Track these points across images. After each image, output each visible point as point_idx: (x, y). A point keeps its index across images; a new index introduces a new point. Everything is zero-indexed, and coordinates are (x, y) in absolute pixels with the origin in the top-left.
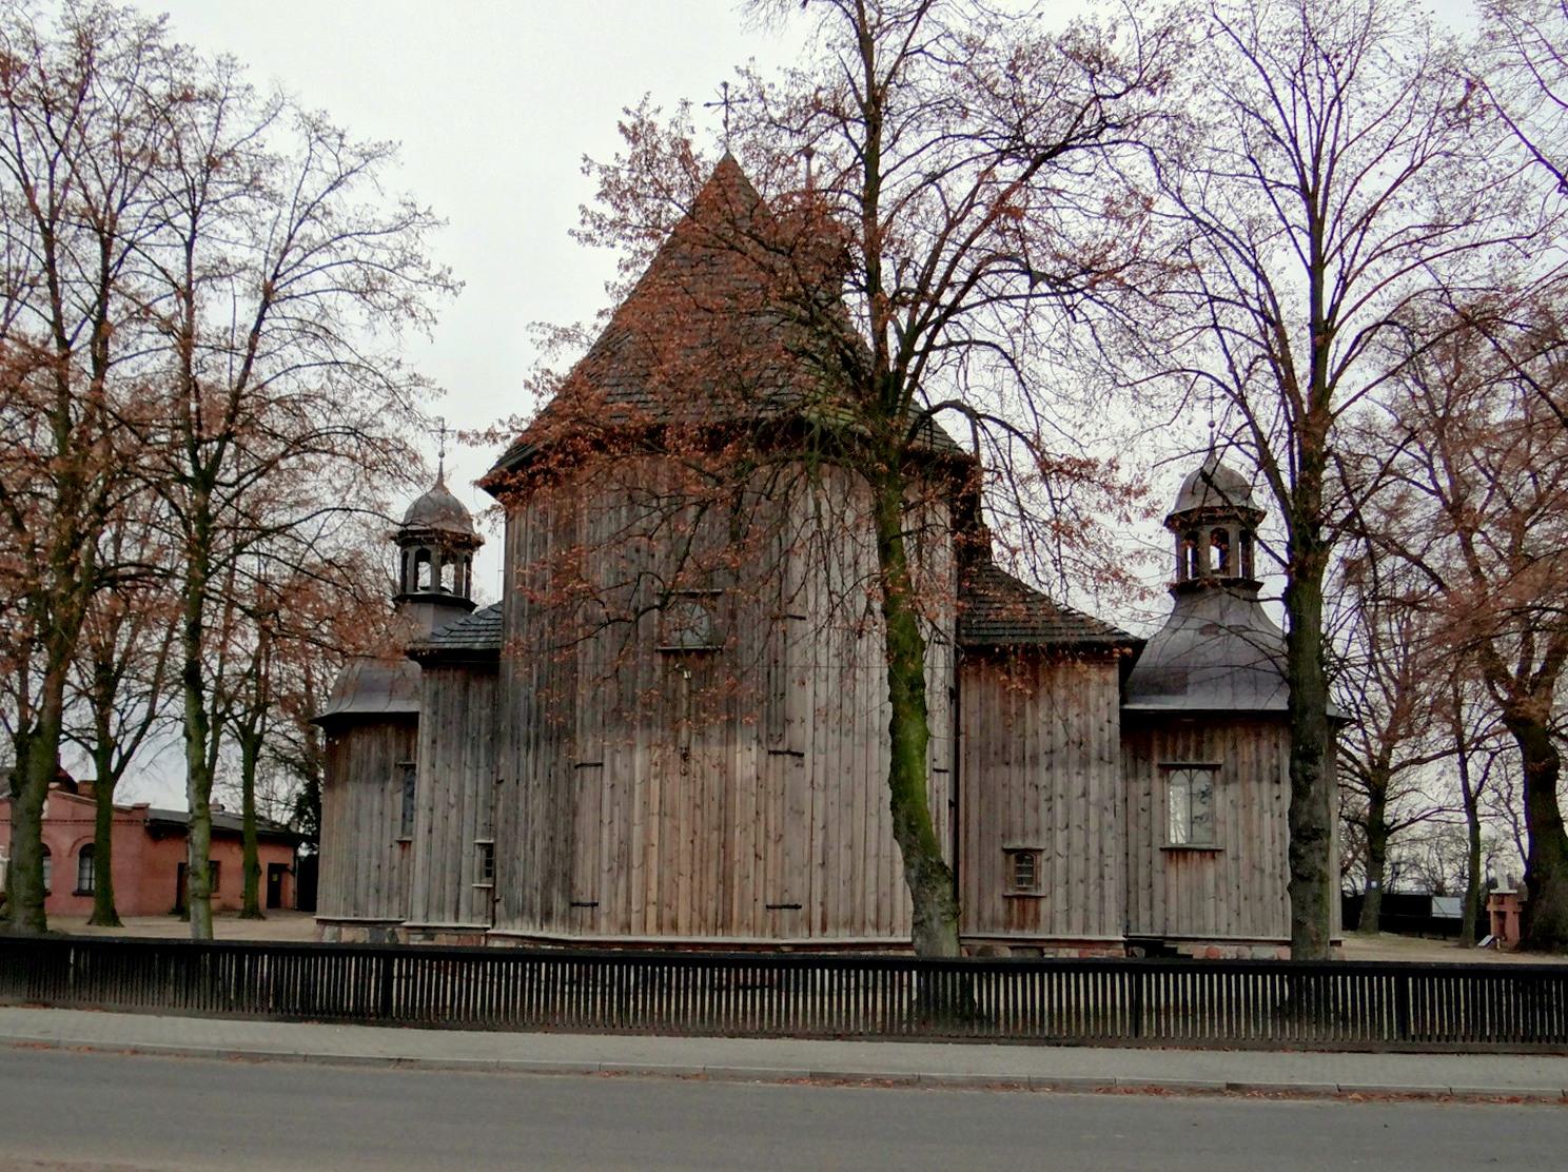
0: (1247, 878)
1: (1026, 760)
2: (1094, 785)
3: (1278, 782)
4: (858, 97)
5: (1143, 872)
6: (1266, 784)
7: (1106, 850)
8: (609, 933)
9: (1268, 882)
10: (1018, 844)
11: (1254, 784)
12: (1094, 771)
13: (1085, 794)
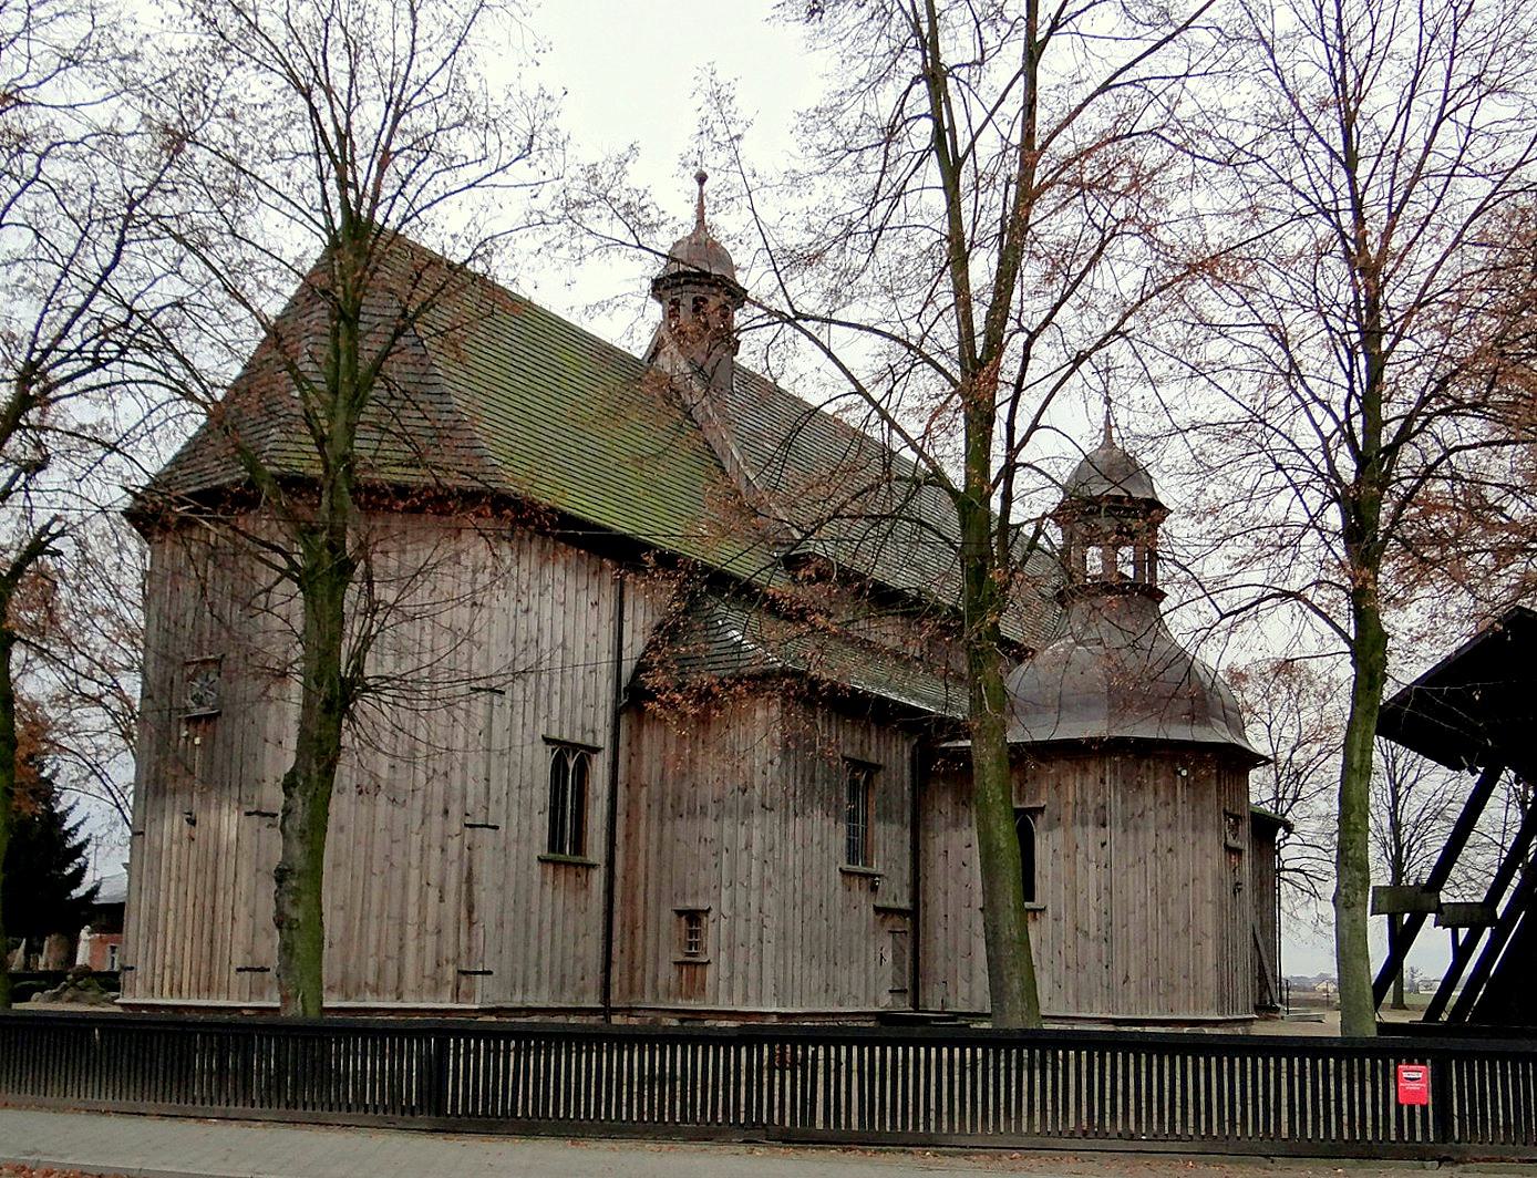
0: (1070, 943)
1: (697, 812)
2: (756, 833)
3: (1104, 825)
4: (1333, 154)
5: (963, 936)
6: (1091, 828)
7: (765, 910)
8: (240, 999)
9: (1093, 946)
10: (690, 904)
11: (1078, 828)
12: (757, 821)
13: (748, 846)
